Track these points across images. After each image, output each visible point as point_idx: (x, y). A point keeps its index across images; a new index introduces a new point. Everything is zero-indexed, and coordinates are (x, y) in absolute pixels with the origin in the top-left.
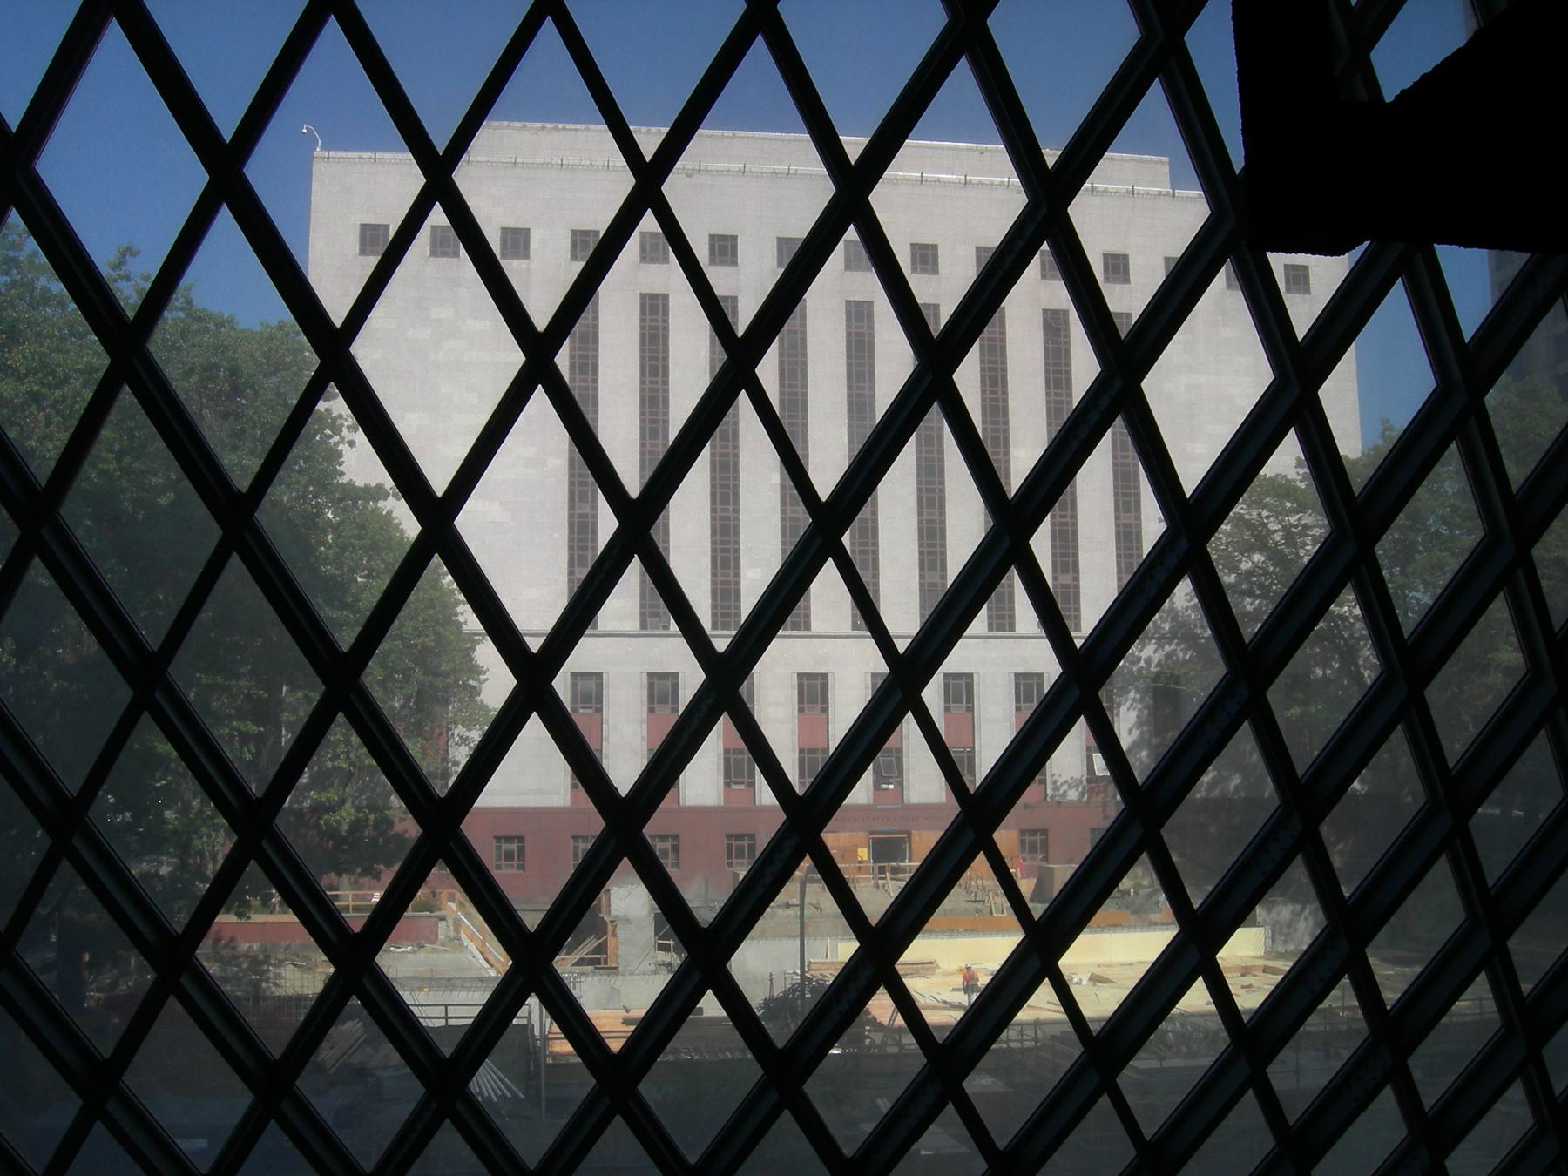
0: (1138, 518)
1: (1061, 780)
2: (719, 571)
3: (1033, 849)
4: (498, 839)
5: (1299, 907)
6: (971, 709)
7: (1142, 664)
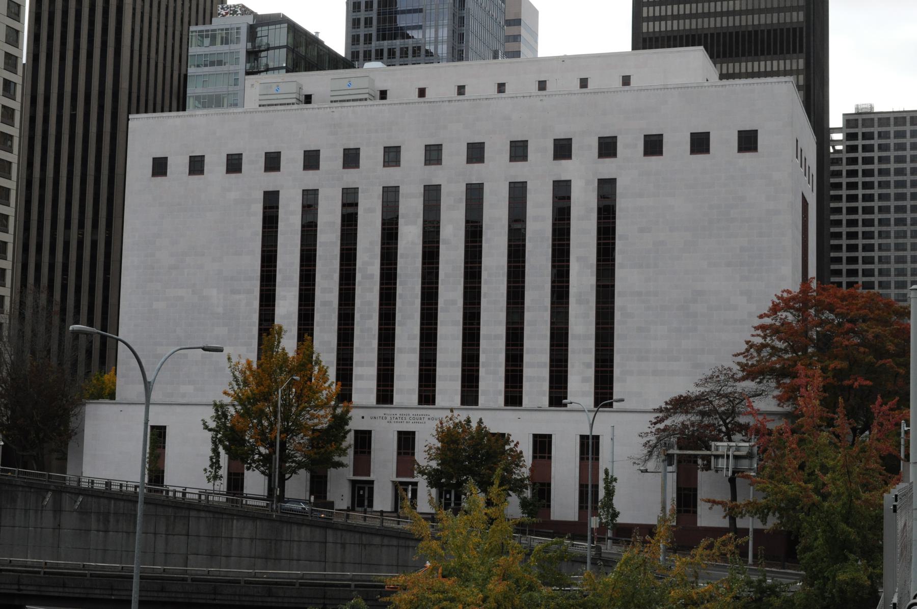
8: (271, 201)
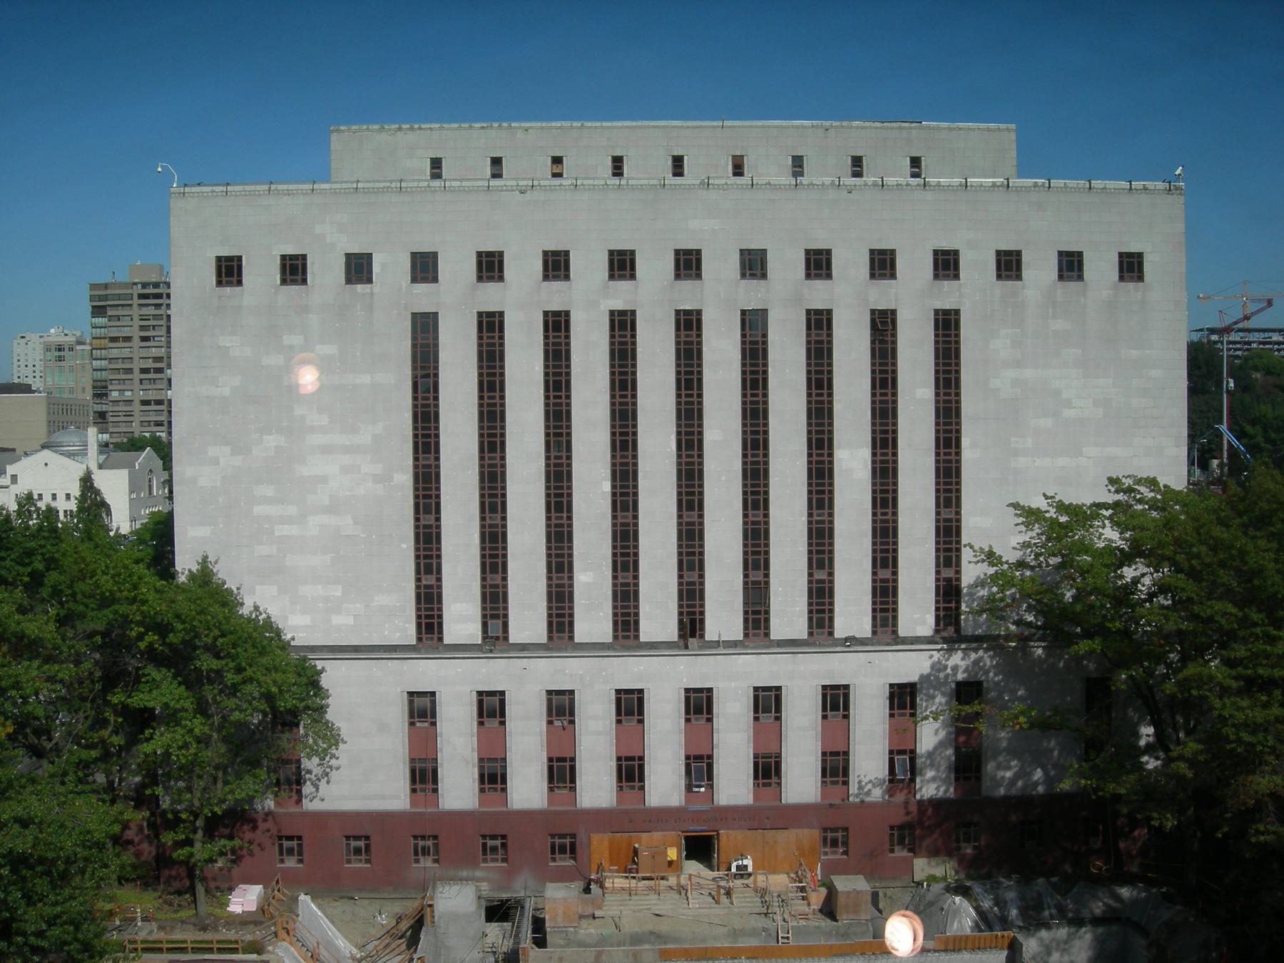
0: (958, 513)
1: (867, 780)
2: (554, 575)
3: (834, 843)
4: (348, 838)
5: (1073, 930)
6: (778, 718)
7: (949, 671)
8: (425, 329)
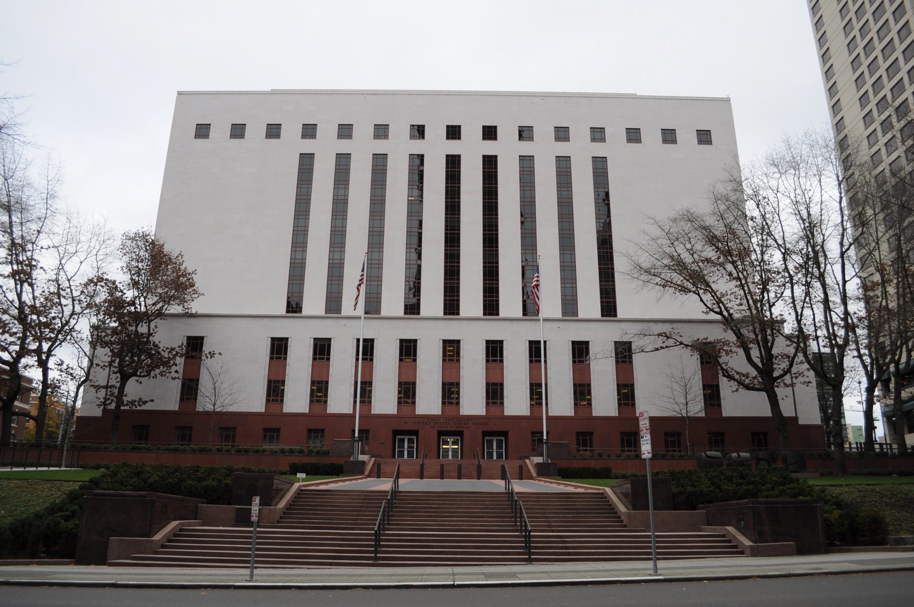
8: (306, 162)
